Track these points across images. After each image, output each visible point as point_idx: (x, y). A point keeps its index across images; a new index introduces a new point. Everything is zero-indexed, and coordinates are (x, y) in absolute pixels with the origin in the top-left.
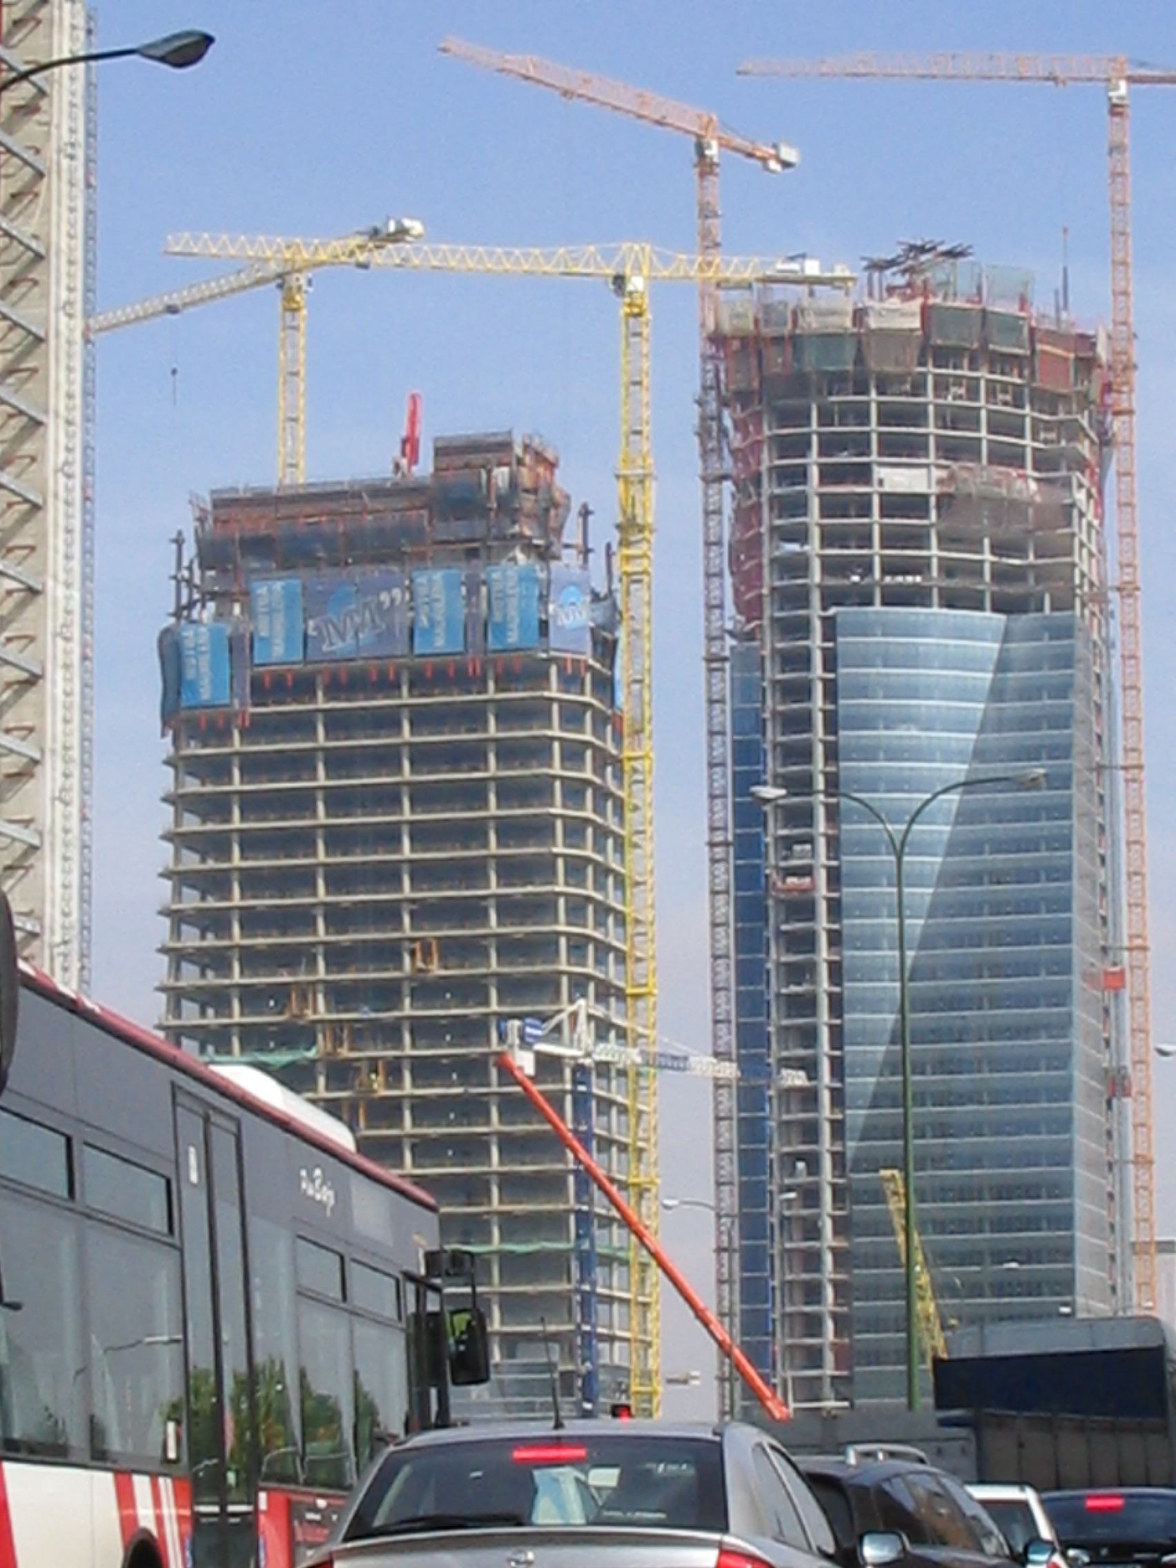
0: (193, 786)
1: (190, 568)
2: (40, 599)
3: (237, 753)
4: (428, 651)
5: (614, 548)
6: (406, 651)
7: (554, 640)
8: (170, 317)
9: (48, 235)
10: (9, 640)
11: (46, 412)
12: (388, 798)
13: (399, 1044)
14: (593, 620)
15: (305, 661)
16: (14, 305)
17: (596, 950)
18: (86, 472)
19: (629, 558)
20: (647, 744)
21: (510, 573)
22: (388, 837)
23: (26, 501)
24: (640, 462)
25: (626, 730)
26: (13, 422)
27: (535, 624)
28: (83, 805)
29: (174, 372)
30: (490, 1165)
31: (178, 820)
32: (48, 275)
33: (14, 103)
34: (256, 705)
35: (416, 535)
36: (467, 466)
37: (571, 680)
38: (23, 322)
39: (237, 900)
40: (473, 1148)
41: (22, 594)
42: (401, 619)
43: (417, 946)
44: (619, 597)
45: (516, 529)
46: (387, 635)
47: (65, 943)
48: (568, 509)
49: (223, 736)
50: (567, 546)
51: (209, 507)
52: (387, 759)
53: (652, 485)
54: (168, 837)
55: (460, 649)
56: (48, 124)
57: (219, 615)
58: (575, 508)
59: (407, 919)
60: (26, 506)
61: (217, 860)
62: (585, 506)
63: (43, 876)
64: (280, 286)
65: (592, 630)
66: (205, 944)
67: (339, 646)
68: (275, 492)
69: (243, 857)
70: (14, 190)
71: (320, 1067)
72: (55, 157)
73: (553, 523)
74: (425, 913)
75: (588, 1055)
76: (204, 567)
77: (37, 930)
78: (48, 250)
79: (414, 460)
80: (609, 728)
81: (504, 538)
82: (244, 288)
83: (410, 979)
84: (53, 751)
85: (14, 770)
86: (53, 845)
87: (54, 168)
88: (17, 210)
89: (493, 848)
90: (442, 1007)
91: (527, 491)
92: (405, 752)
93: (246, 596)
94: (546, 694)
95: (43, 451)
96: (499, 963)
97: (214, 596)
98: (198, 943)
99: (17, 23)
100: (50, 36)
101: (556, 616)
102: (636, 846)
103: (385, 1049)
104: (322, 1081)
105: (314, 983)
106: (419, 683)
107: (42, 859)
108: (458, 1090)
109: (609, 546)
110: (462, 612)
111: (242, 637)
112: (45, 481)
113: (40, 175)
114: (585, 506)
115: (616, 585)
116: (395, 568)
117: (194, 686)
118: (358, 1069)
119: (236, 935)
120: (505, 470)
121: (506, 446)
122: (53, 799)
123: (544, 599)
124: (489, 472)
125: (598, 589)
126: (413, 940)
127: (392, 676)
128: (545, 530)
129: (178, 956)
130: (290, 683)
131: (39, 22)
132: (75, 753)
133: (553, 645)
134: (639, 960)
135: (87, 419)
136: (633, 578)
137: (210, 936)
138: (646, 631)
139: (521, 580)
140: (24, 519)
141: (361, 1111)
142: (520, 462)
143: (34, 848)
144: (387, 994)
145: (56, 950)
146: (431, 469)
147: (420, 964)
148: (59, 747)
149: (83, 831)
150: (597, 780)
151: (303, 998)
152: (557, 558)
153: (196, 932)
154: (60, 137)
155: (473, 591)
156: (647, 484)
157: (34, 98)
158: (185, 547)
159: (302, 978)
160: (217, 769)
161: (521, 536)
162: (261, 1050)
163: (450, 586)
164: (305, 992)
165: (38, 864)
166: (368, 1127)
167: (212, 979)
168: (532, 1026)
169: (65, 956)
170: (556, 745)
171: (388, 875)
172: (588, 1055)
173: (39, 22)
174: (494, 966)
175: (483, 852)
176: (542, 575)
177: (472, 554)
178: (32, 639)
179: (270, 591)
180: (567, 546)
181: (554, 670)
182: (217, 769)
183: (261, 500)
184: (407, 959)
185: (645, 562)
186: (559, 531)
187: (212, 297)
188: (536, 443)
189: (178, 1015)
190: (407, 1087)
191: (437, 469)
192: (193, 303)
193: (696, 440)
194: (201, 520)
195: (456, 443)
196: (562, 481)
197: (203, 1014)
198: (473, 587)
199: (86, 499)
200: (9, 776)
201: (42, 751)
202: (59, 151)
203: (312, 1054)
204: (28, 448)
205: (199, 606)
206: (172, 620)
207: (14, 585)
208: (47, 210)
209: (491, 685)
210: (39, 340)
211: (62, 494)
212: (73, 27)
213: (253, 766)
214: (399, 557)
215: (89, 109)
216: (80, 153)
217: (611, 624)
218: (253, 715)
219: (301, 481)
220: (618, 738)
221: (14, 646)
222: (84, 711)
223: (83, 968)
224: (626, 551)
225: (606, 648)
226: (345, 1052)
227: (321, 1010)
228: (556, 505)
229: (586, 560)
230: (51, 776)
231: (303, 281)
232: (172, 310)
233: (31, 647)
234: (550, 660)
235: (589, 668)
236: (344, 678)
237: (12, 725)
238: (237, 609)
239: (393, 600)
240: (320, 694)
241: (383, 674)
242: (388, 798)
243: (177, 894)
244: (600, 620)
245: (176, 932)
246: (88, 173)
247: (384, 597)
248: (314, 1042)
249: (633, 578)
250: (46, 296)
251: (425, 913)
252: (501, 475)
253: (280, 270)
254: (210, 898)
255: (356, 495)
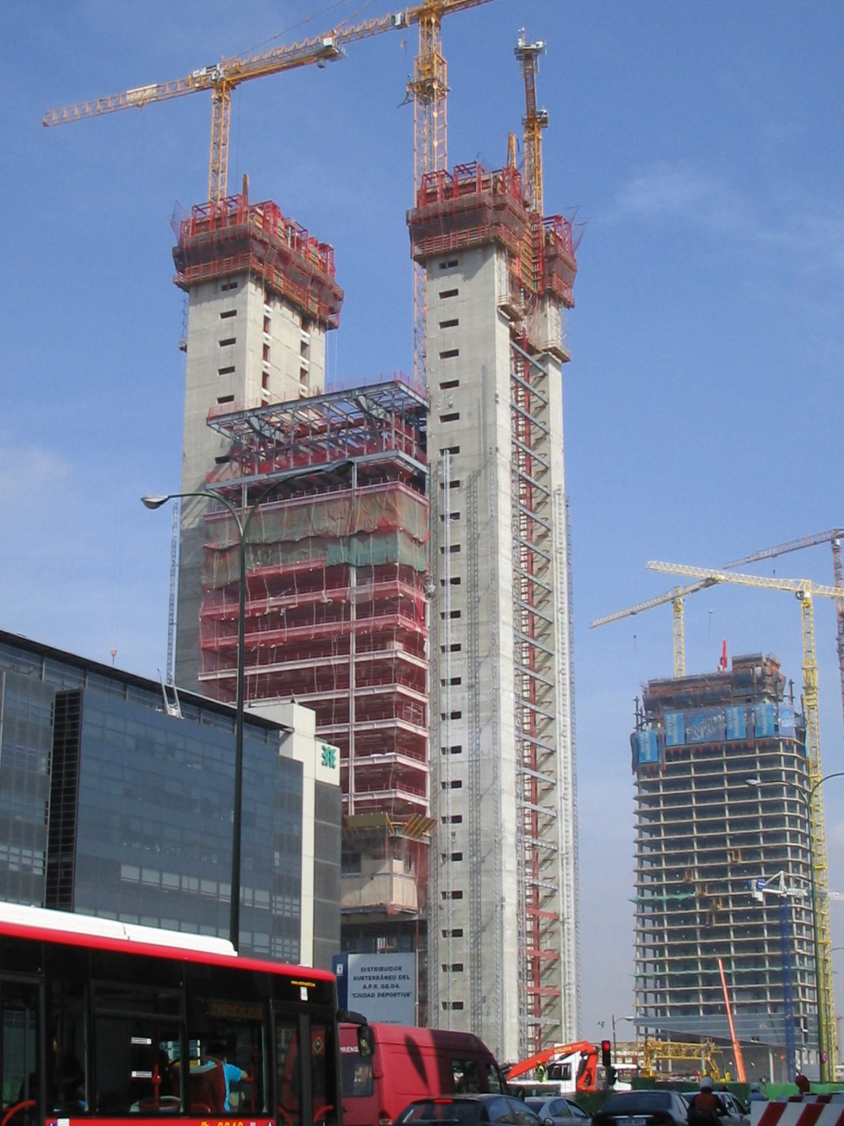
0: (646, 793)
1: (641, 711)
2: (554, 721)
3: (661, 780)
4: (733, 738)
5: (804, 697)
6: (724, 739)
7: (781, 732)
8: (632, 616)
9: (553, 583)
10: (543, 737)
11: (554, 650)
12: (719, 795)
13: (727, 890)
14: (796, 724)
15: (686, 744)
16: (540, 611)
17: (802, 852)
18: (571, 672)
19: (808, 700)
20: (819, 771)
21: (763, 708)
22: (720, 810)
23: (547, 684)
24: (811, 663)
25: (810, 766)
26: (542, 654)
27: (773, 726)
28: (574, 801)
30: (764, 936)
31: (640, 806)
32: (553, 598)
33: (539, 534)
34: (668, 761)
35: (726, 694)
36: (745, 667)
37: (788, 748)
38: (544, 616)
39: (663, 837)
40: (758, 930)
41: (547, 720)
42: (722, 727)
43: (733, 852)
44: (806, 715)
45: (765, 690)
47: (567, 853)
48: (785, 682)
49: (656, 774)
50: (785, 696)
51: (648, 687)
52: (719, 780)
53: (816, 672)
54: (636, 813)
55: (745, 737)
56: (552, 541)
57: (653, 728)
58: (788, 681)
59: (728, 842)
60: (547, 686)
61: (655, 821)
62: (791, 680)
63: (557, 828)
64: (673, 602)
65: (796, 728)
66: (652, 853)
68: (672, 680)
69: (665, 820)
70: (539, 567)
71: (697, 900)
72: (554, 554)
73: (779, 688)
74: (735, 839)
75: (785, 893)
76: (646, 710)
77: (556, 849)
78: (553, 588)
79: (725, 666)
80: (804, 766)
81: (761, 694)
82: (660, 604)
83: (730, 865)
84: (561, 780)
85: (546, 788)
86: (561, 816)
87: (554, 558)
88: (541, 574)
89: (761, 813)
90: (744, 876)
91: (769, 676)
92: (725, 778)
93: (662, 720)
94: (779, 753)
95: (554, 665)
96: (765, 858)
97: (651, 720)
98: (650, 853)
99: (539, 504)
100: (551, 509)
102: (817, 811)
103: (722, 892)
104: (698, 905)
105: (693, 868)
106: (730, 751)
107: (557, 821)
108: (750, 908)
109: (802, 696)
110: (744, 723)
111: (661, 736)
112: (554, 676)
113: (549, 560)
114: (791, 680)
115: (805, 711)
116: (719, 708)
117: (644, 755)
118: (711, 901)
119: (664, 850)
121: (759, 659)
122: (561, 798)
123: (776, 717)
124: (753, 669)
125: (797, 712)
126: (731, 850)
128: (776, 690)
129: (641, 859)
130: (672, 754)
131: (547, 503)
132: (570, 780)
134: (819, 855)
135: (571, 652)
136: (811, 708)
137: (654, 850)
138: (817, 728)
139: (767, 710)
140: (547, 691)
141: (713, 918)
142: (765, 665)
143: (554, 818)
144: (722, 871)
145: (564, 857)
146: (731, 669)
147: (734, 859)
148: (563, 778)
149: (574, 810)
150: (800, 786)
151: (690, 873)
152: (781, 701)
153: (649, 849)
154: (556, 546)
155: (749, 715)
156: (814, 671)
157: (546, 532)
158: (639, 703)
159: (689, 866)
160: (654, 786)
161: (767, 693)
162: (674, 894)
163: (739, 713)
164: (690, 871)
165: (556, 824)
166: (717, 923)
167: (655, 867)
168: (761, 882)
169: (567, 858)
170: (783, 773)
171: (721, 825)
172: (785, 893)
173: (547, 503)
174: (763, 859)
175: (756, 815)
176: (775, 708)
177: (749, 701)
178: (551, 737)
179: (672, 718)
180: (785, 696)
181: (781, 744)
182: (654, 786)
183: (668, 684)
184: (729, 857)
185: (815, 701)
186: (782, 691)
187: (648, 608)
188: (771, 657)
189: (643, 881)
190: (731, 907)
191: (734, 669)
192: (641, 610)
193: (837, 654)
194: (645, 692)
195: (740, 659)
196: (781, 671)
197: (653, 880)
198: (749, 712)
199: (571, 683)
200: (544, 790)
201: (556, 780)
202: (556, 551)
203: (693, 895)
204: (548, 664)
205: (645, 724)
206: (635, 730)
207: (544, 717)
208: (552, 574)
209: (757, 751)
210: (551, 623)
211: (561, 681)
212: (560, 504)
213: (668, 785)
214: (720, 703)
215: (568, 535)
216: (565, 552)
217: (804, 725)
218: (667, 765)
219: (684, 675)
220: (808, 770)
221: (546, 739)
222: (573, 764)
223: (575, 863)
224: (807, 697)
225: (802, 735)
226: (706, 894)
227: (697, 878)
228: (780, 681)
229: (792, 701)
230: (559, 790)
231: (681, 600)
232: (633, 613)
233: (551, 740)
234: (781, 740)
235: (795, 743)
236: (701, 750)
237: (544, 770)
238: (659, 725)
239: (718, 719)
240: (692, 756)
242: (719, 795)
243: (641, 835)
244: (799, 724)
245: (641, 849)
246: (568, 559)
247: (715, 718)
248: (694, 890)
249: (811, 708)
250: (553, 605)
251: (735, 839)
252: (758, 670)
253: (672, 596)
254: (653, 836)
255: (703, 680)
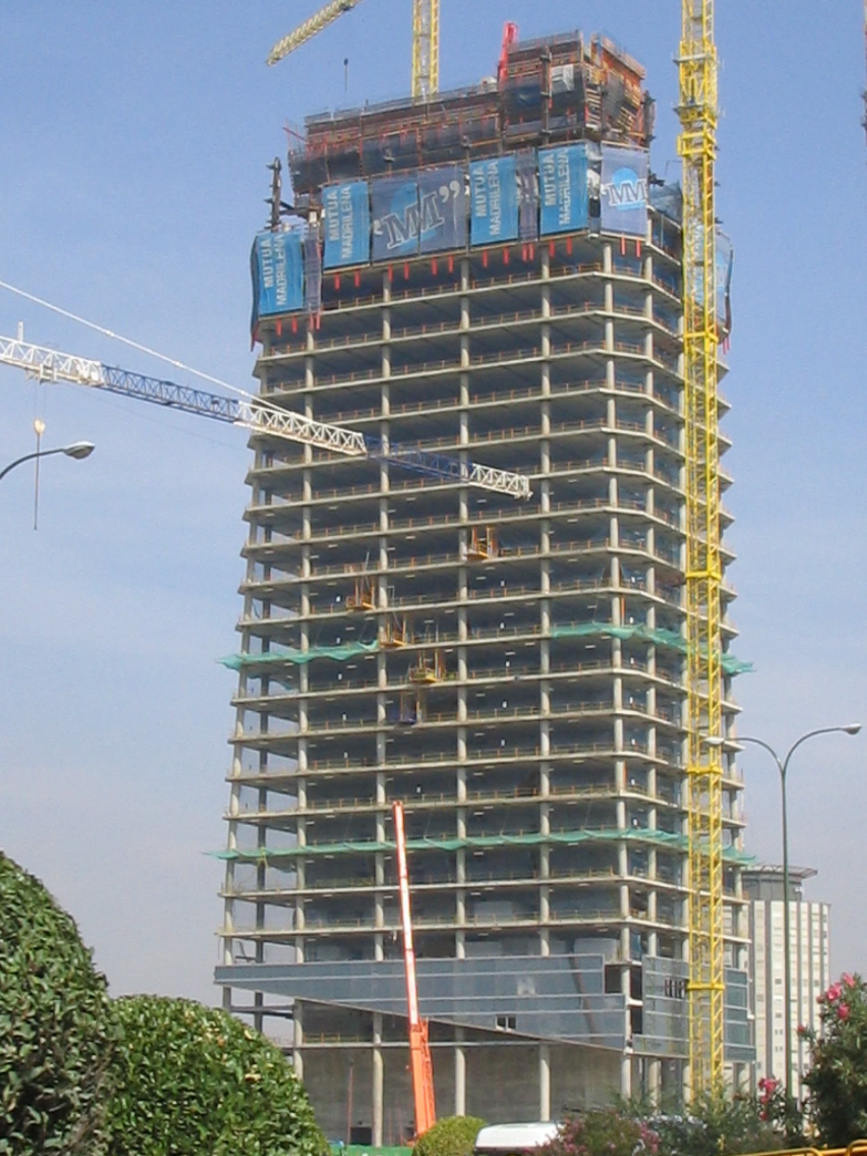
29: (346, 62)
46: (445, 230)
49: (299, 340)
67: (403, 242)
101: (607, 197)
106: (479, 275)
120: (571, 66)
127: (451, 269)
133: (604, 224)
159: (365, 572)
164: (369, 587)
181: (608, 251)
188: (608, 44)
203: (372, 648)
226: (405, 645)
241: (443, 268)
